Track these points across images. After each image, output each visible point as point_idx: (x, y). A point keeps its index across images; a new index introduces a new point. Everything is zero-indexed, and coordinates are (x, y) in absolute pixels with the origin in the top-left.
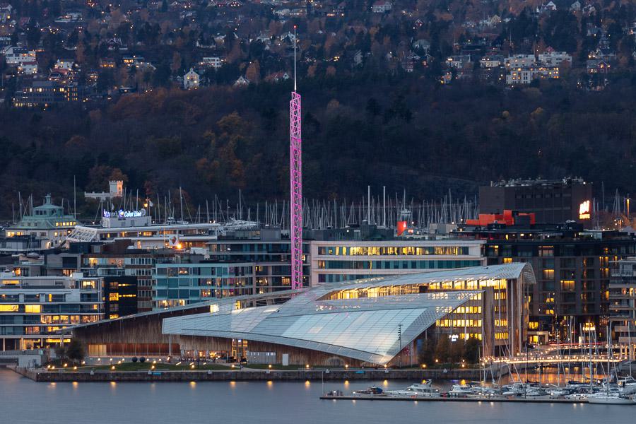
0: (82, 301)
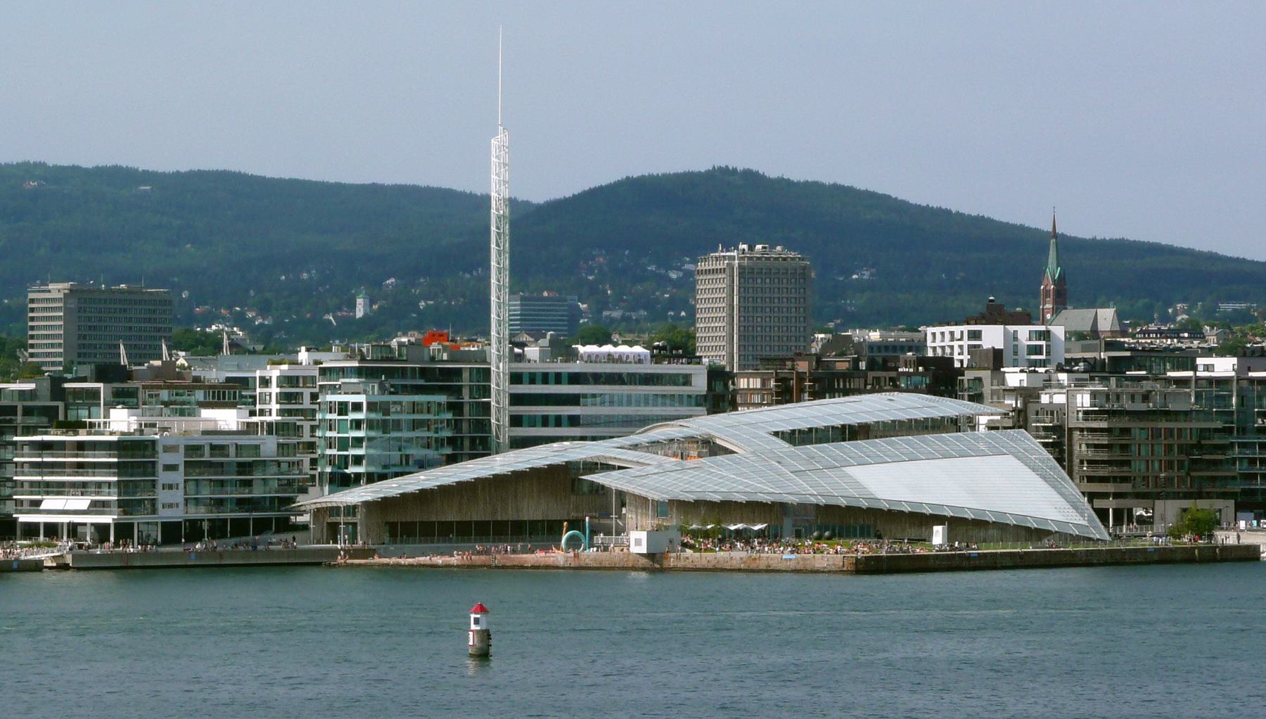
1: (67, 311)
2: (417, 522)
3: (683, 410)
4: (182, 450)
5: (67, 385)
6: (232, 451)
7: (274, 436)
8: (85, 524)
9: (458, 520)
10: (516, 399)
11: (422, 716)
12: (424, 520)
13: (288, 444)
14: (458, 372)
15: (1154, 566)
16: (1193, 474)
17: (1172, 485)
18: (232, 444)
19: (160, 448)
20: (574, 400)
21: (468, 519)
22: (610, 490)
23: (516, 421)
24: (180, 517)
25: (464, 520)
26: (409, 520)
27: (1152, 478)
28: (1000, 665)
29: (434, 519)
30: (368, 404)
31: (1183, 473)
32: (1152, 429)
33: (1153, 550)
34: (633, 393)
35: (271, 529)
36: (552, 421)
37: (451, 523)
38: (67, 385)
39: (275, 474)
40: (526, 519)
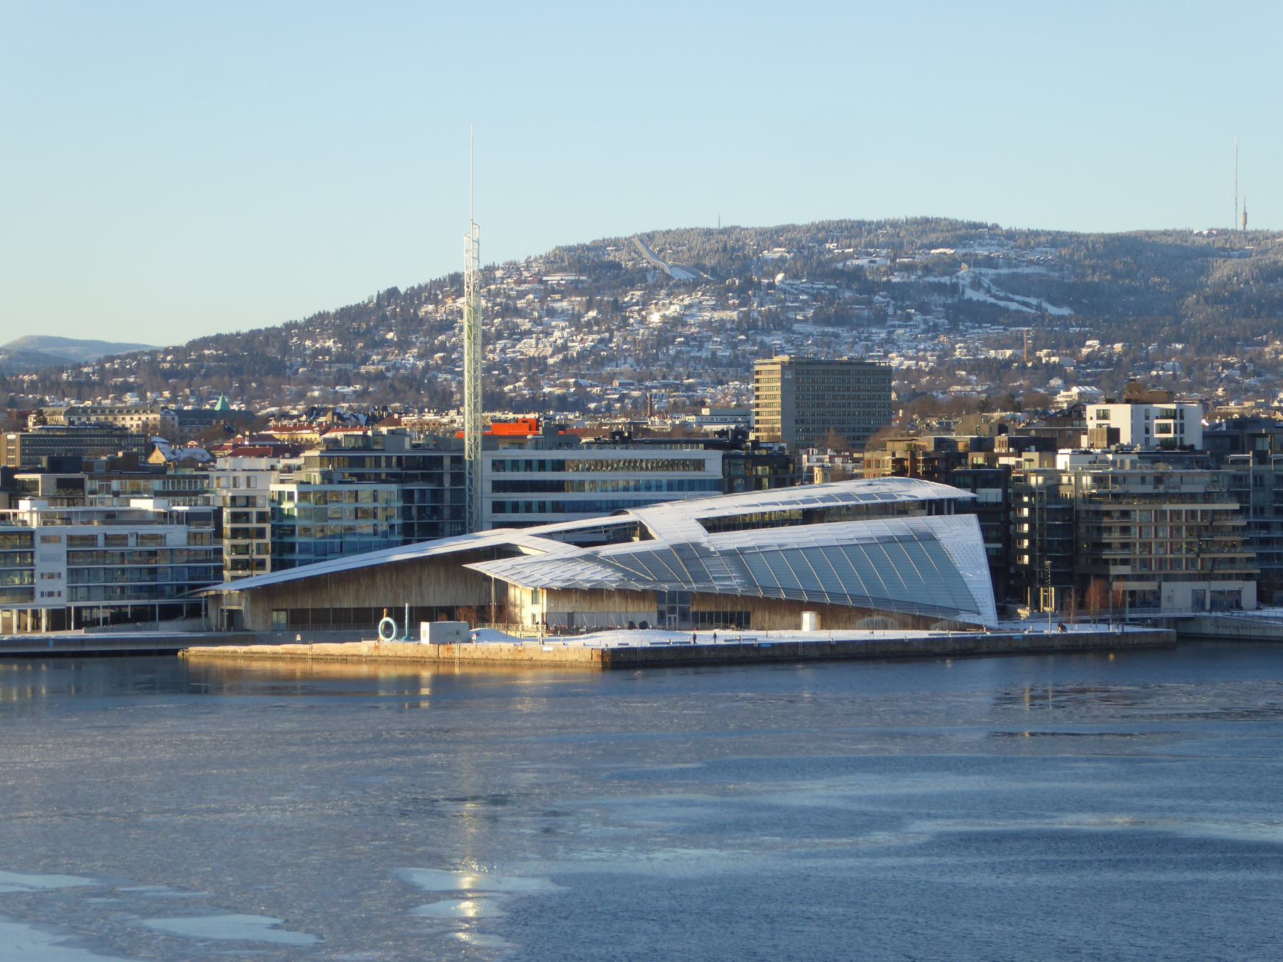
0: (189, 544)
1: (783, 380)
2: (308, 609)
3: (664, 494)
4: (64, 541)
5: (16, 476)
6: (101, 540)
7: (185, 526)
8: (127, 606)
9: (356, 607)
10: (498, 486)
11: (1044, 734)
12: (317, 607)
13: (201, 534)
14: (441, 459)
15: (832, 666)
16: (1201, 556)
17: (1180, 566)
18: (132, 535)
19: (37, 539)
20: (559, 486)
21: (367, 605)
22: (490, 578)
23: (498, 507)
24: (63, 605)
25: (362, 606)
26: (299, 607)
27: (1156, 562)
28: (887, 750)
29: (327, 606)
30: (300, 493)
31: (1192, 555)
32: (1156, 511)
33: (1021, 638)
34: (641, 478)
35: (182, 614)
36: (535, 507)
37: (348, 610)
38: (16, 476)
39: (187, 562)
40: (432, 605)
